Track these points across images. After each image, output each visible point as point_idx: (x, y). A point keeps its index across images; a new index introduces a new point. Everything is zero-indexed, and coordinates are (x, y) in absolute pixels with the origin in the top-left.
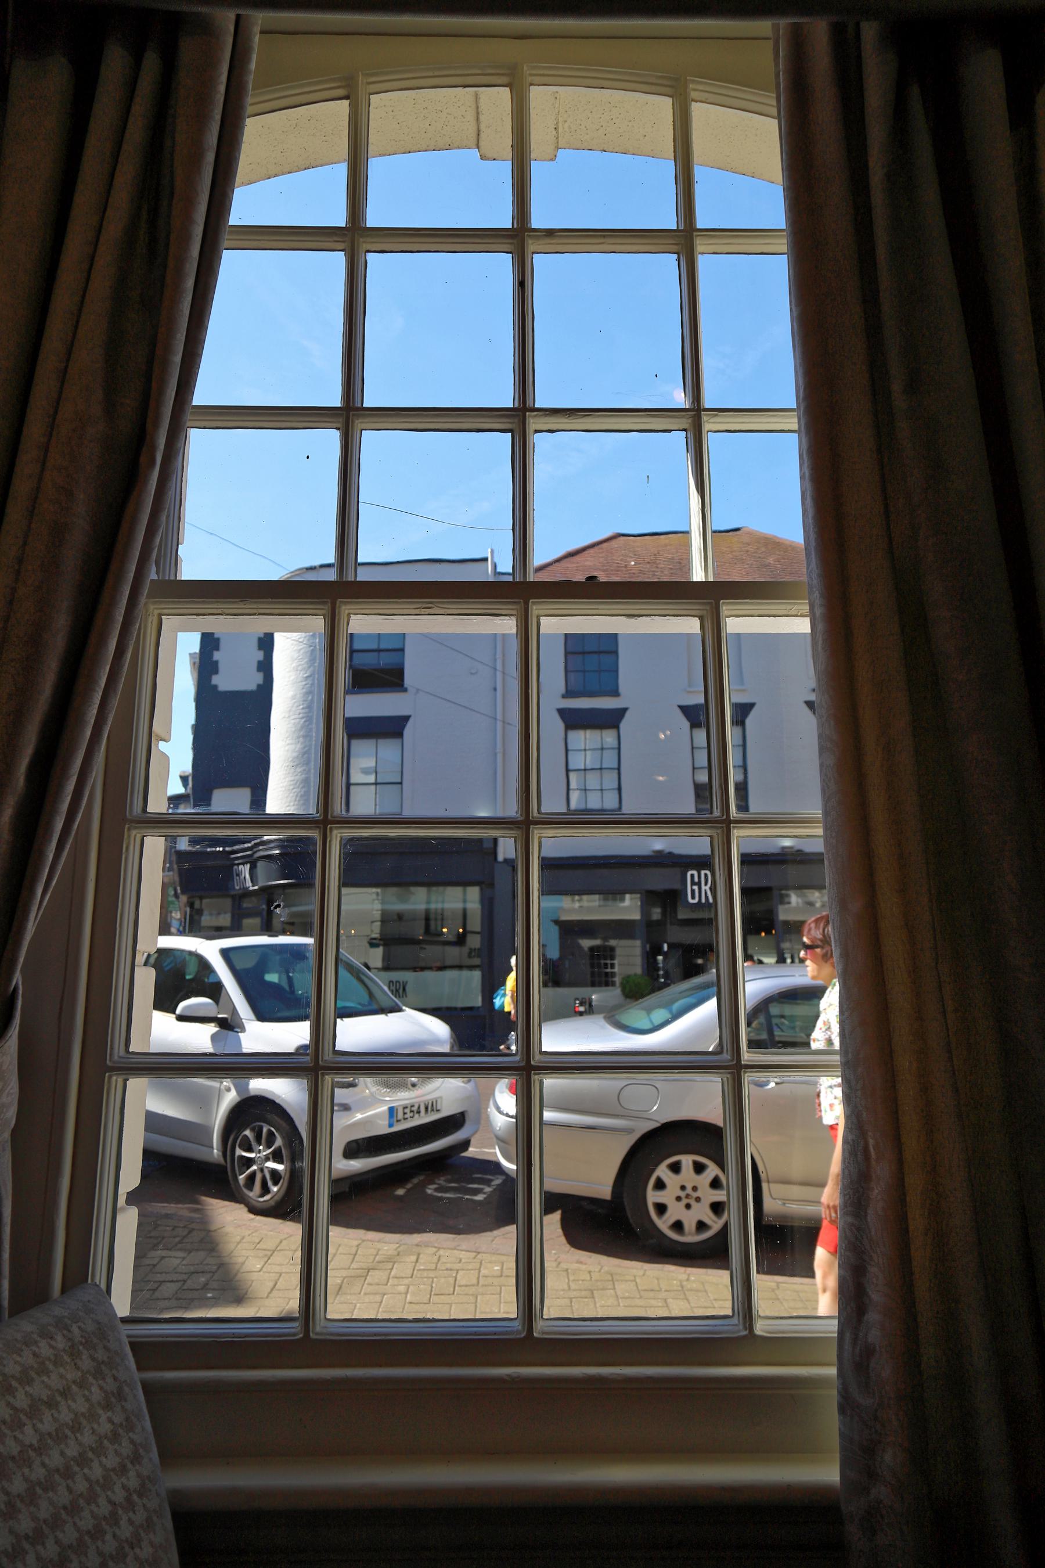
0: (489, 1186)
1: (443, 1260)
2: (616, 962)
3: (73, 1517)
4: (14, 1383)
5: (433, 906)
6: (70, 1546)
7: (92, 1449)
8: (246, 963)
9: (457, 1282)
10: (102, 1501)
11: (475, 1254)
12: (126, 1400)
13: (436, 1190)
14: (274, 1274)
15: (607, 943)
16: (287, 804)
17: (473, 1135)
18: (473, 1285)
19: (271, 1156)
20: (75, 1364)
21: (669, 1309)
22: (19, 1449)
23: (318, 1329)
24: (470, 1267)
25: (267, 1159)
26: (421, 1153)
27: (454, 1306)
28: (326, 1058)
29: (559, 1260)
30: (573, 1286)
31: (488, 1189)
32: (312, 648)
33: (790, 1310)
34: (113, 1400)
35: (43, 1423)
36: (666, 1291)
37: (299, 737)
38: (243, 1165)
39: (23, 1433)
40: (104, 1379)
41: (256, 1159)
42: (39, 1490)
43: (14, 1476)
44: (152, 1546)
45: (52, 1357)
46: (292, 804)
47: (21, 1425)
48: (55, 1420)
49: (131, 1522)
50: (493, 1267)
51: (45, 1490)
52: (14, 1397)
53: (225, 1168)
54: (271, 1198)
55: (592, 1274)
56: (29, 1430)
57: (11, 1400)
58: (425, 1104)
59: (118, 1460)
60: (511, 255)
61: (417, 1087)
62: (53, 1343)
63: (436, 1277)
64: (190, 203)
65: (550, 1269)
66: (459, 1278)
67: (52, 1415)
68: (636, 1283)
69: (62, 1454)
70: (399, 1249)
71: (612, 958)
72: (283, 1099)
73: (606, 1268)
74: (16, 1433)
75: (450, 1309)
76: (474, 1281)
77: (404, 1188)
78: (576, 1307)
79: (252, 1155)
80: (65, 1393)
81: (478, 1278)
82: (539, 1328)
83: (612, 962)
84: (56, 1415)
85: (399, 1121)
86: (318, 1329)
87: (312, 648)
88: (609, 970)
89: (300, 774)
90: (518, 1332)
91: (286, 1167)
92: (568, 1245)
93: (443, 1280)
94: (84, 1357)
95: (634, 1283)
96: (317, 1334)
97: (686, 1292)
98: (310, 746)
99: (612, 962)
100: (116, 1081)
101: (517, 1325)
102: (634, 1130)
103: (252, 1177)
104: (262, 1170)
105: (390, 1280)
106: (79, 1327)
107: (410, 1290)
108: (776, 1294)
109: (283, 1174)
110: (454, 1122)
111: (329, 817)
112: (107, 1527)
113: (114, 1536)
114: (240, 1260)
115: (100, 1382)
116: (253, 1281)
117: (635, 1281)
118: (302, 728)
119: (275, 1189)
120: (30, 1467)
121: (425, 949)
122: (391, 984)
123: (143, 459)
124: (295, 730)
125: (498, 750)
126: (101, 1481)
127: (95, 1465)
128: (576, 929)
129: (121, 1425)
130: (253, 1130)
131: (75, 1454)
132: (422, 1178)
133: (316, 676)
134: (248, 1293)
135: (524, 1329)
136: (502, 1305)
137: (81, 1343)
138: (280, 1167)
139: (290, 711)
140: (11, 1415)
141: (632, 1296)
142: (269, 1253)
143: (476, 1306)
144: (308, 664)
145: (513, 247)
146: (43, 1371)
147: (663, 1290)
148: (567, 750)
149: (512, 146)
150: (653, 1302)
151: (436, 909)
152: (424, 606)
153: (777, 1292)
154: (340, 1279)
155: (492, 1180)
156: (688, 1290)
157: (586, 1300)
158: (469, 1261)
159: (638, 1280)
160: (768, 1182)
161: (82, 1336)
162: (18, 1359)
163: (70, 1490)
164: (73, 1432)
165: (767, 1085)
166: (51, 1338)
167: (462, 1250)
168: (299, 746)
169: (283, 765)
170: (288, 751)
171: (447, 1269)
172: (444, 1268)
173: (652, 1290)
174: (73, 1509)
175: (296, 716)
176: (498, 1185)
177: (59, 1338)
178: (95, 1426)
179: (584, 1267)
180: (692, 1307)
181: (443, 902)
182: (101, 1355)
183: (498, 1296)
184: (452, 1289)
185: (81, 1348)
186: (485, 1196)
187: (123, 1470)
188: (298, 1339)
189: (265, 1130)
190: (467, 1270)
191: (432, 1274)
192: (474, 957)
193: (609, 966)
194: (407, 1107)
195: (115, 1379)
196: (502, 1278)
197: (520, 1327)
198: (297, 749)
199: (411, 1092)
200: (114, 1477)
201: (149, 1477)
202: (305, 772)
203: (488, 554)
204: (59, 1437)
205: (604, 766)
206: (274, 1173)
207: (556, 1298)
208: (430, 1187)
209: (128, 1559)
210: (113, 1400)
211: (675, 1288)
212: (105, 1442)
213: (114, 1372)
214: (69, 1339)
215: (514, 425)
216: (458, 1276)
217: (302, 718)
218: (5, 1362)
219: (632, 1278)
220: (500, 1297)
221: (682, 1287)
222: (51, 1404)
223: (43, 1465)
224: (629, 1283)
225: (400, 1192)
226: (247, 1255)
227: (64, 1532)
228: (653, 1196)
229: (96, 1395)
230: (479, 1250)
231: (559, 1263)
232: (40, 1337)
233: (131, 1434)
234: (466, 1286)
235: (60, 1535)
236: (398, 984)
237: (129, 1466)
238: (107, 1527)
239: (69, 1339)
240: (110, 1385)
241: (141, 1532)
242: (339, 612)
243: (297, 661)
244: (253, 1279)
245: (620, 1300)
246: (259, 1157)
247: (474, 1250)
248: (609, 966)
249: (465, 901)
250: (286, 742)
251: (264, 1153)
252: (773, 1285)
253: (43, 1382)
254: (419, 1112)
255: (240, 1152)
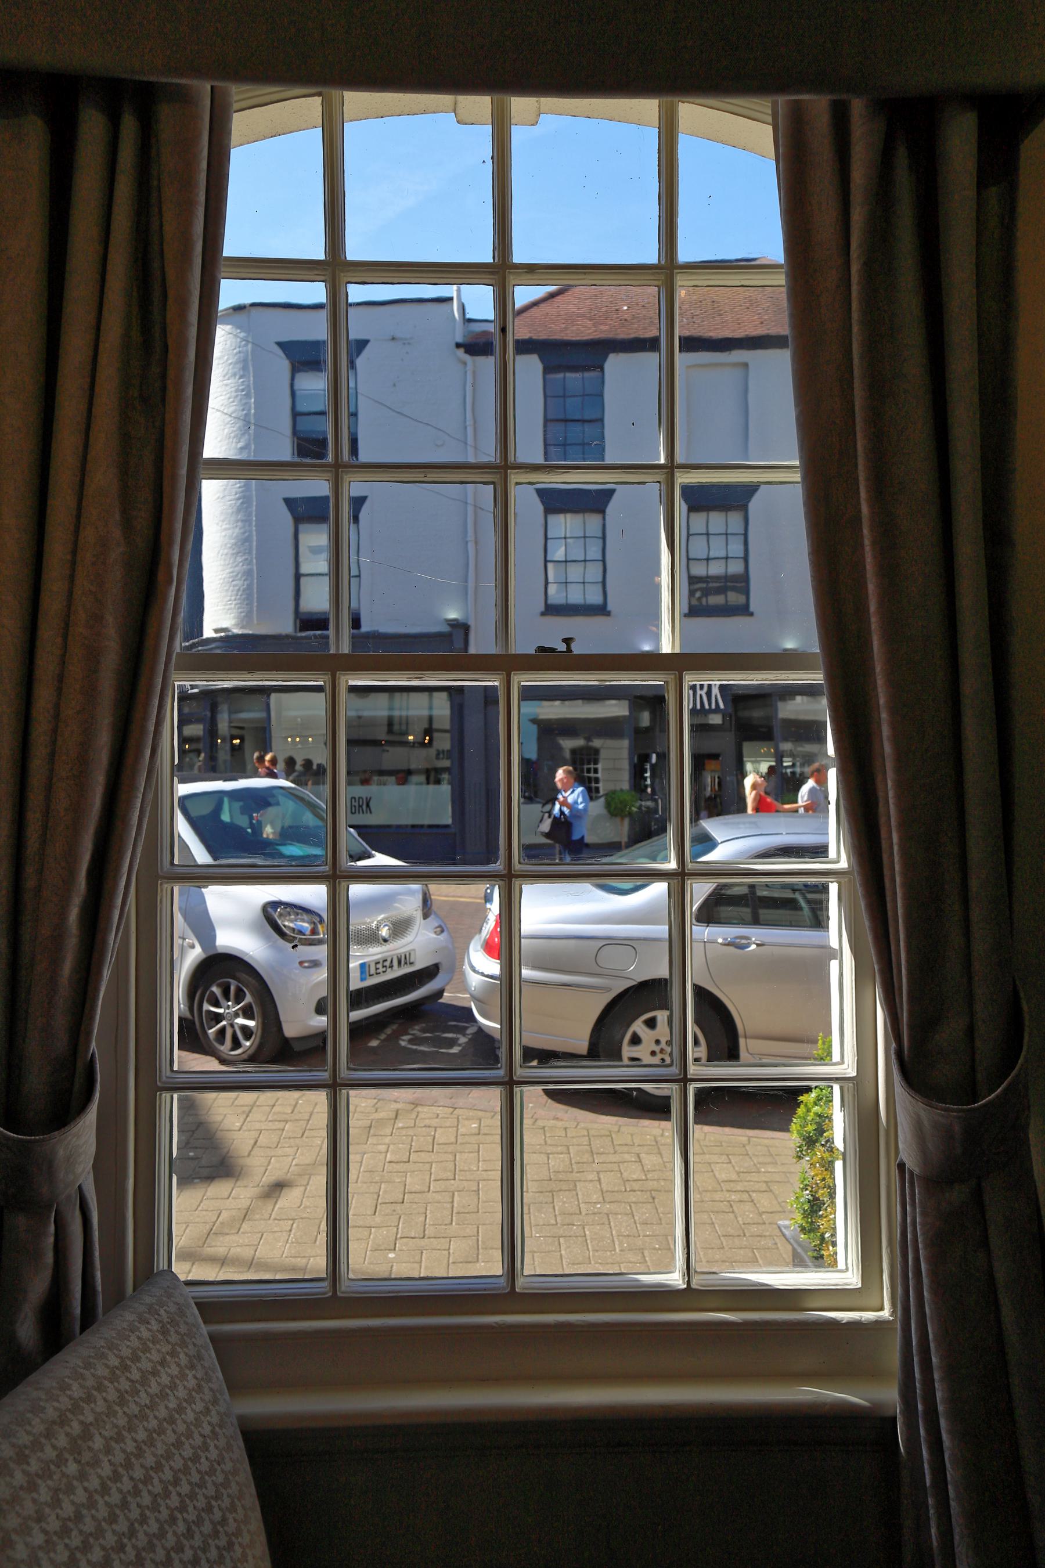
0: (464, 1035)
1: (421, 1116)
2: (599, 766)
3: (178, 1450)
4: (129, 1363)
5: (396, 713)
6: (180, 1470)
7: (185, 1401)
8: (202, 810)
9: (436, 1140)
10: (196, 1436)
11: (452, 1110)
12: (204, 1360)
13: (410, 1041)
14: (254, 1132)
15: (591, 744)
16: (229, 598)
17: (446, 985)
18: (452, 1143)
19: (240, 1013)
20: (167, 1340)
21: (642, 1165)
22: (139, 1409)
23: (343, 1289)
24: (448, 1124)
25: (236, 1015)
26: (395, 1005)
27: (434, 1165)
28: (342, 1075)
29: (533, 1120)
30: (549, 1141)
31: (463, 1040)
32: (245, 412)
33: (758, 1165)
34: (195, 1361)
35: (151, 1388)
36: (639, 1146)
37: (237, 521)
38: (212, 1020)
39: (139, 1397)
40: (187, 1347)
41: (225, 1015)
42: (155, 1435)
43: (138, 1429)
44: (232, 1461)
45: (151, 1338)
46: (233, 598)
47: (138, 1392)
48: (159, 1384)
49: (216, 1447)
50: (471, 1125)
51: (159, 1435)
52: (130, 1373)
53: (194, 1023)
54: (243, 1053)
55: (568, 1130)
56: (143, 1394)
57: (129, 1375)
58: (398, 957)
59: (203, 1404)
60: (492, 288)
61: (389, 942)
62: (150, 1327)
63: (415, 1135)
64: (183, 303)
65: (527, 1126)
66: (437, 1136)
67: (156, 1380)
68: (612, 1138)
69: (167, 1407)
70: (376, 1106)
71: (596, 762)
72: (251, 957)
73: (582, 1125)
74: (136, 1399)
75: (431, 1168)
76: (453, 1140)
77: (378, 1039)
78: (553, 1164)
79: (221, 1011)
80: (163, 1363)
81: (457, 1137)
82: (520, 1284)
83: (596, 766)
84: (159, 1381)
85: (373, 975)
86: (343, 1289)
87: (245, 412)
88: (592, 775)
89: (241, 564)
90: (504, 1289)
91: (257, 1023)
92: (545, 1096)
93: (422, 1139)
94: (172, 1333)
95: (610, 1138)
96: (343, 1293)
97: (661, 1147)
98: (251, 531)
99: (596, 766)
100: (166, 1096)
101: (503, 1282)
102: (611, 989)
103: (222, 1032)
104: (232, 1025)
105: (369, 1139)
106: (165, 1310)
107: (390, 1149)
108: (746, 1150)
109: (254, 1030)
110: (430, 973)
111: (338, 872)
112: (201, 1454)
113: (207, 1459)
114: (219, 1118)
115: (185, 1349)
116: (234, 1140)
117: (611, 1136)
118: (238, 511)
119: (248, 1044)
120: (147, 1420)
121: (388, 751)
122: (353, 800)
123: (161, 576)
124: (233, 513)
125: (469, 539)
126: (194, 1422)
127: (189, 1411)
128: (557, 732)
129: (202, 1379)
130: (219, 985)
131: (175, 1406)
132: (395, 1027)
133: (253, 447)
134: (230, 1152)
135: (508, 1286)
136: (480, 1164)
137: (168, 1323)
138: (251, 1023)
139: (225, 489)
140: (130, 1386)
141: (607, 1152)
142: (247, 1109)
143: (455, 1164)
144: (241, 431)
145: (494, 281)
146: (146, 1350)
147: (636, 1144)
148: (546, 538)
149: (492, 158)
150: (627, 1157)
151: (401, 717)
152: (416, 676)
153: (747, 1148)
154: (319, 1139)
155: (466, 1028)
156: (661, 1145)
157: (562, 1156)
158: (446, 1116)
159: (613, 1136)
160: (746, 1037)
161: (168, 1318)
162: (129, 1343)
163: (174, 1432)
164: (171, 1391)
165: (750, 947)
166: (148, 1323)
167: (439, 1106)
168: (237, 530)
169: (219, 552)
170: (225, 536)
171: (425, 1126)
172: (423, 1125)
173: (626, 1145)
174: (178, 1445)
175: (233, 497)
176: (473, 1034)
177: (153, 1322)
178: (186, 1383)
179: (559, 1124)
180: (664, 1162)
181: (408, 709)
182: (183, 1329)
183: (476, 1154)
184: (431, 1147)
185: (168, 1326)
186: (460, 1048)
187: (207, 1411)
188: (327, 1297)
189: (233, 988)
190: (446, 1127)
191: (411, 1132)
192: (443, 759)
193: (592, 771)
194: (379, 963)
195: (194, 1345)
196: (480, 1136)
197: (505, 1284)
198: (235, 534)
199: (384, 947)
200: (202, 1417)
201: (225, 1413)
202: (246, 562)
203: (453, 293)
204: (163, 1396)
205: (587, 559)
206: (244, 1029)
207: (533, 1153)
208: (404, 1038)
209: (218, 1473)
210: (195, 1361)
211: (649, 1143)
212: (193, 1393)
213: (193, 1340)
214: (160, 1322)
215: (494, 281)
216: (437, 1134)
217: (238, 499)
218: (120, 1348)
219: (608, 1133)
220: (479, 1155)
221: (657, 1142)
222: (155, 1373)
223: (156, 1417)
224: (604, 1138)
225: (374, 1043)
226: (225, 1113)
227: (174, 1461)
228: (628, 1051)
229: (183, 1360)
230: (456, 1106)
231: (536, 1120)
232: (140, 1323)
233: (209, 1384)
234: (446, 1144)
235: (172, 1463)
236: (361, 800)
237: (211, 1407)
238: (201, 1454)
239: (160, 1322)
240: (192, 1351)
241: (224, 1453)
242: (339, 683)
243: (228, 426)
244: (235, 1137)
245: (595, 1156)
246: (228, 1013)
247: (450, 1105)
248: (592, 771)
249: (431, 708)
250: (221, 526)
251: (234, 1010)
252: (744, 1139)
253: (147, 1358)
254: (391, 967)
255: (207, 1007)
